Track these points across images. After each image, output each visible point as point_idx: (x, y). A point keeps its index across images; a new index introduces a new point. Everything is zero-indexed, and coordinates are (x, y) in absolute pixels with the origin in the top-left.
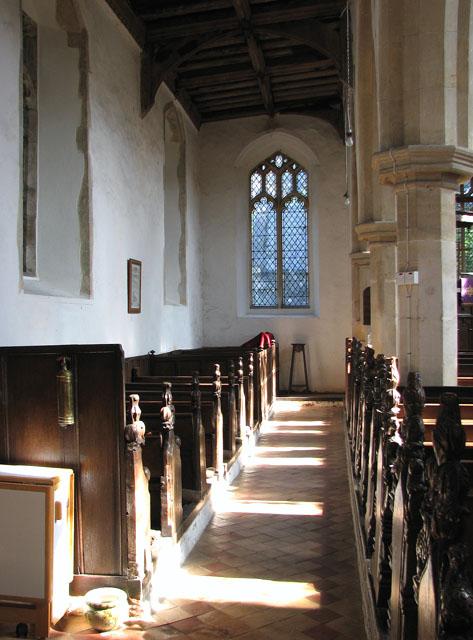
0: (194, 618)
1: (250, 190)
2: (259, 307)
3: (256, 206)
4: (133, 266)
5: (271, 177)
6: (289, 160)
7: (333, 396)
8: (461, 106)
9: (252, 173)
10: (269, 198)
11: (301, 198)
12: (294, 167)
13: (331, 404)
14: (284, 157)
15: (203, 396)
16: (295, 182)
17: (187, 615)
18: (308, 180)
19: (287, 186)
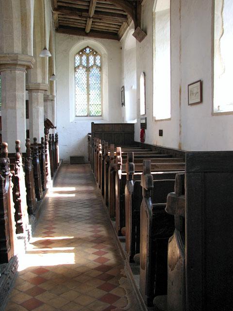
0: (16, 261)
1: (75, 63)
2: (93, 116)
3: (77, 70)
4: (199, 83)
5: (84, 58)
6: (93, 50)
7: (39, 173)
8: (106, 29)
9: (75, 55)
10: (97, 66)
11: (97, 66)
12: (95, 53)
13: (49, 178)
14: (90, 48)
15: (134, 153)
16: (81, 60)
17: (10, 257)
18: (101, 59)
19: (91, 62)
